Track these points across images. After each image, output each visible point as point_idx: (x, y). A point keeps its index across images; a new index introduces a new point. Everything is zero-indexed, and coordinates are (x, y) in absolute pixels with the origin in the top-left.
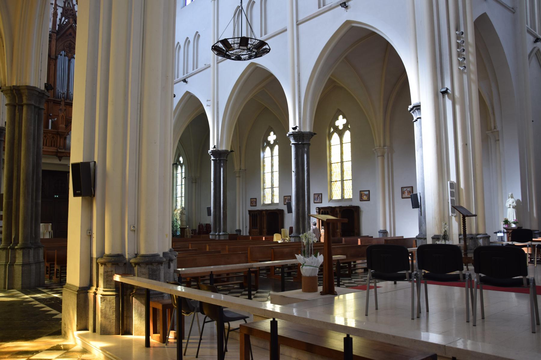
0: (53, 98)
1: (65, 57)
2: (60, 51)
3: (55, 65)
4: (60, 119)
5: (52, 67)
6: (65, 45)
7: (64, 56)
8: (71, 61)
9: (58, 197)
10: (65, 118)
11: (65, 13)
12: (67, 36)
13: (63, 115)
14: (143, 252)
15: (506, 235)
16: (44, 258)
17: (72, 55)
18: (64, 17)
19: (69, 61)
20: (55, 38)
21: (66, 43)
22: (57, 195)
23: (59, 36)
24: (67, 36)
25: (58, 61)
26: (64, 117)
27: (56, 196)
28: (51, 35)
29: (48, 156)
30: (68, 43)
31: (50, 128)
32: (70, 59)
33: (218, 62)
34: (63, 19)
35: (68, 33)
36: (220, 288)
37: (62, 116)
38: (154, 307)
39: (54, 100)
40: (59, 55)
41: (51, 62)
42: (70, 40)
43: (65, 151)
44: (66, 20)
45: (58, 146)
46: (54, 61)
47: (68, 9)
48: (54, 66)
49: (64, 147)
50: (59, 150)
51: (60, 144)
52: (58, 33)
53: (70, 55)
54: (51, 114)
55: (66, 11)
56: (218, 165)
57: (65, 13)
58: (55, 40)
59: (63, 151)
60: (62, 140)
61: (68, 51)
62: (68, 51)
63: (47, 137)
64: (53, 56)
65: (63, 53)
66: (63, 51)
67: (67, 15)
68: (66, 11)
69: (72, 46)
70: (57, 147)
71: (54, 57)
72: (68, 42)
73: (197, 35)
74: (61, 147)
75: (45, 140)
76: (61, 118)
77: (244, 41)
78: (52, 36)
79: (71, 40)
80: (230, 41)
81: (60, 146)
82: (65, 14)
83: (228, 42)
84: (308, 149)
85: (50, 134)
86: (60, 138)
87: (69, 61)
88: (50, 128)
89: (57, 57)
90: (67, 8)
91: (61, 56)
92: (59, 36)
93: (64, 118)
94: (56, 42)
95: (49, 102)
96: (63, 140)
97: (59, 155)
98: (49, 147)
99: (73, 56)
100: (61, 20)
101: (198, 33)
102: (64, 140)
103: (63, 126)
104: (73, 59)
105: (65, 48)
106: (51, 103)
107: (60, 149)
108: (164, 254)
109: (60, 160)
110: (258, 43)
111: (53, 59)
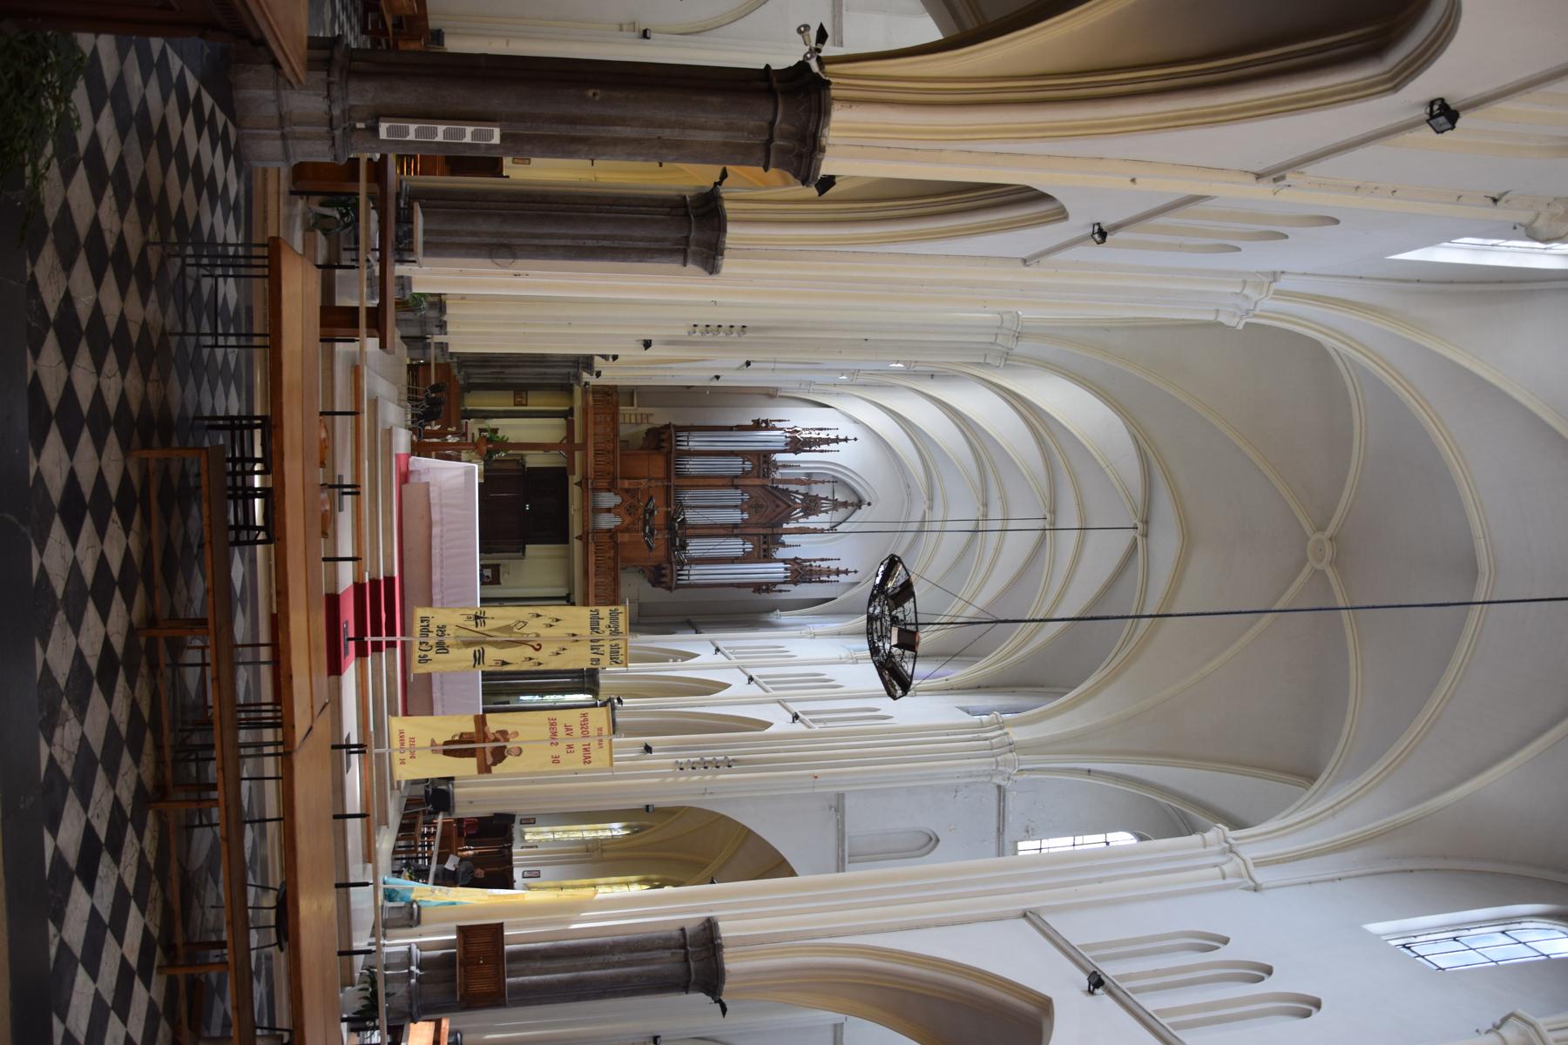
3: (723, 486)
14: (447, 302)
15: (210, 777)
16: (353, 341)
24: (774, 502)
25: (733, 491)
29: (682, 37)
31: (455, 950)
33: (783, 703)
35: (778, 502)
36: (223, 1000)
44: (798, 501)
50: (590, 535)
53: (746, 506)
56: (576, 675)
64: (736, 482)
65: (746, 497)
70: (595, 478)
71: (735, 483)
72: (764, 503)
77: (908, 642)
80: (909, 605)
83: (907, 599)
84: (805, 561)
87: (736, 507)
88: (455, 950)
89: (736, 487)
100: (797, 492)
107: (593, 536)
108: (445, 322)
110: (906, 672)
111: (733, 481)
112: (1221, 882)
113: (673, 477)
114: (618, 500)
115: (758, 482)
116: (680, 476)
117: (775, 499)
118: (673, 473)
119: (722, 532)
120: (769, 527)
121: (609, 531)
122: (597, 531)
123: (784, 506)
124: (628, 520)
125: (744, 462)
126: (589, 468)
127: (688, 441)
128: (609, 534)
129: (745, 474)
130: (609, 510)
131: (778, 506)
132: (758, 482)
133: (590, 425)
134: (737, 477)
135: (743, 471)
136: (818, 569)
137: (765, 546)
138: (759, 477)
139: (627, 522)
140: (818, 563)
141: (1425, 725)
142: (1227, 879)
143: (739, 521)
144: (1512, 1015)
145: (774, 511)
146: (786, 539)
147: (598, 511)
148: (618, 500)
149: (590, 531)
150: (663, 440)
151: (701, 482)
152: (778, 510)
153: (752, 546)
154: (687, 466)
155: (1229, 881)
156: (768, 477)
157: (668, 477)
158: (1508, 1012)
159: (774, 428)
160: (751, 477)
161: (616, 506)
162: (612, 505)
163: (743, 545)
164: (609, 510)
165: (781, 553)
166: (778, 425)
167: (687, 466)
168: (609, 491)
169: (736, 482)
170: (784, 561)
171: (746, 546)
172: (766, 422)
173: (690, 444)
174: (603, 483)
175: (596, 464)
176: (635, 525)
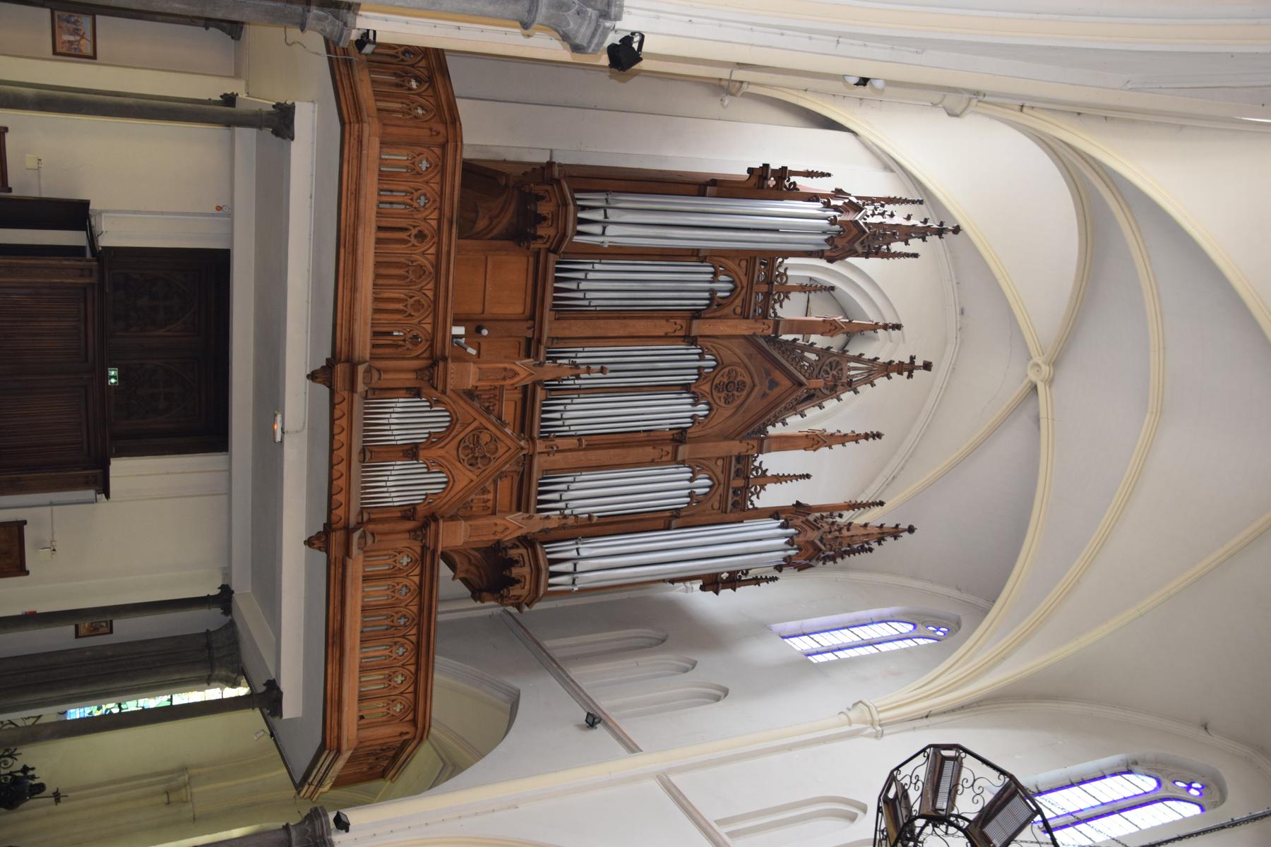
0: (548, 338)
1: (695, 371)
2: (715, 352)
4: (501, 365)
5: (662, 327)
6: (739, 369)
7: (699, 368)
8: (684, 395)
9: (114, 385)
10: (502, 386)
11: (831, 359)
12: (768, 373)
13: (516, 374)
17: (704, 396)
18: (817, 358)
19: (686, 387)
20: (759, 332)
21: (742, 371)
22: (120, 377)
23: (762, 342)
24: (768, 373)
25: (681, 348)
26: (512, 378)
27: (112, 377)
28: (766, 318)
30: (745, 379)
32: (693, 389)
34: (813, 357)
35: (778, 376)
37: (512, 370)
38: (715, 594)
39: (539, 341)
40: (700, 351)
41: (679, 322)
42: (754, 386)
43: (356, 397)
45: (371, 527)
46: (682, 333)
47: (841, 370)
48: (662, 334)
49: (374, 389)
51: (386, 371)
52: (774, 340)
53: (706, 388)
54: (485, 332)
55: (837, 366)
57: (831, 359)
58: (750, 332)
59: (361, 387)
60: (408, 379)
61: (717, 381)
62: (717, 381)
63: (416, 314)
66: (714, 363)
67: (824, 367)
68: (837, 366)
69: (735, 392)
70: (373, 357)
71: (694, 332)
72: (748, 380)
73: (855, 810)
74: (370, 541)
75: (400, 306)
76: (505, 369)
78: (765, 321)
79: (756, 390)
81: (379, 370)
82: (828, 362)
85: (429, 328)
86: (416, 371)
87: (686, 387)
89: (691, 340)
90: (843, 366)
91: (697, 357)
92: (762, 342)
93: (504, 379)
94: (744, 337)
95: (531, 322)
96: (408, 385)
97: (340, 369)
98: (373, 325)
99: (702, 399)
101: (860, 813)
102: (407, 389)
103: (471, 381)
104: (690, 401)
105: (726, 370)
106: (528, 328)
107: (368, 371)
109: (313, 376)
111: (689, 328)
112: (847, 729)
113: (548, 315)
114: (438, 420)
115: (744, 328)
116: (564, 311)
117: (768, 366)
118: (549, 302)
119: (650, 452)
120: (749, 437)
121: (408, 512)
122: (373, 517)
123: (785, 383)
124: (465, 475)
125: (715, 274)
126: (358, 327)
127: (605, 224)
128: (410, 525)
129: (715, 306)
130: (411, 452)
131: (773, 384)
132: (744, 328)
133: (370, 185)
134: (696, 314)
135: (711, 299)
136: (863, 531)
137: (739, 483)
138: (745, 316)
139: (462, 482)
140: (848, 516)
141: (1128, 489)
142: (853, 725)
143: (686, 423)
144: (860, 702)
145: (765, 395)
146: (772, 462)
147: (376, 454)
148: (438, 420)
149: (353, 520)
150: (541, 219)
151: (615, 328)
152: (776, 391)
153: (708, 482)
154: (583, 285)
155: (855, 727)
156: (765, 315)
157: (534, 316)
158: (857, 701)
159: (794, 193)
160: (725, 317)
161: (434, 440)
162: (420, 436)
163: (691, 480)
164: (411, 452)
165: (771, 497)
166: (804, 184)
167: (583, 285)
168: (416, 393)
169: (698, 328)
170: (774, 513)
171: (697, 482)
172: (783, 173)
173: (611, 230)
174: (402, 371)
175: (376, 311)
176: (484, 491)
